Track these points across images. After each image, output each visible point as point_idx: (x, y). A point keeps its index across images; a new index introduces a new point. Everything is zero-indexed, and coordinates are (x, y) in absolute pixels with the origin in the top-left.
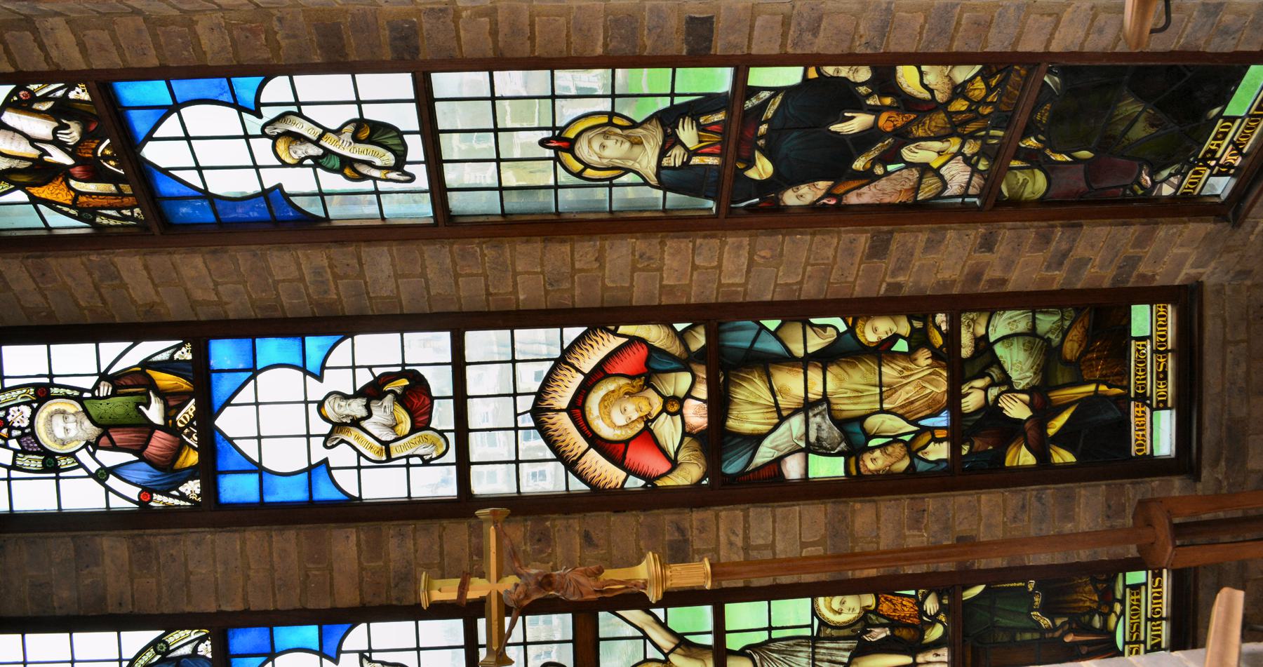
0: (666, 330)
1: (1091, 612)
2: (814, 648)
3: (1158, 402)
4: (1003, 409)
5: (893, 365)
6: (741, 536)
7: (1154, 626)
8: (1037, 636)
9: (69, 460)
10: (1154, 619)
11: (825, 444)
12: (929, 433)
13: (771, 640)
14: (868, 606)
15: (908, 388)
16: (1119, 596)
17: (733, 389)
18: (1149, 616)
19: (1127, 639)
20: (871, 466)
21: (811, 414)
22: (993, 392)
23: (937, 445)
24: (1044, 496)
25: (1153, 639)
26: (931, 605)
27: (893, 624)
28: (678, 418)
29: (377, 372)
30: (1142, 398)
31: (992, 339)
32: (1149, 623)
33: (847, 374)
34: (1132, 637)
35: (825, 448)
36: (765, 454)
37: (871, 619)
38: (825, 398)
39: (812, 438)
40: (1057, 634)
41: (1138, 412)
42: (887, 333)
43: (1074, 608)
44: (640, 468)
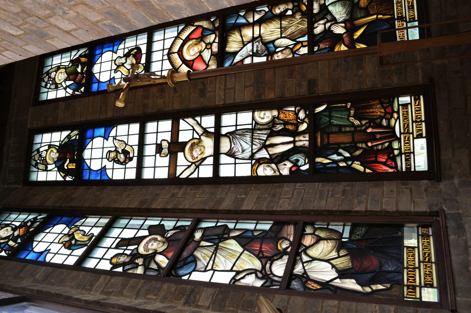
0: (208, 22)
1: (381, 118)
2: (253, 133)
3: (410, 19)
4: (333, 30)
5: (286, 20)
6: (223, 85)
7: (417, 125)
8: (352, 129)
9: (60, 85)
10: (417, 121)
11: (259, 52)
12: (300, 43)
13: (237, 130)
14: (275, 116)
15: (292, 28)
16: (396, 109)
17: (228, 37)
18: (414, 120)
19: (402, 131)
20: (276, 58)
21: (254, 42)
22: (328, 25)
23: (304, 48)
24: (348, 60)
25: (418, 132)
26: (302, 115)
27: (286, 123)
28: (210, 50)
29: (129, 49)
30: (401, 18)
31: (327, 4)
32: (414, 124)
33: (268, 25)
34: (405, 131)
35: (260, 54)
36: (238, 58)
37: (276, 121)
38: (260, 36)
39: (255, 51)
40: (363, 128)
41: (399, 24)
42: (284, 9)
43: (372, 116)
44: (197, 68)
